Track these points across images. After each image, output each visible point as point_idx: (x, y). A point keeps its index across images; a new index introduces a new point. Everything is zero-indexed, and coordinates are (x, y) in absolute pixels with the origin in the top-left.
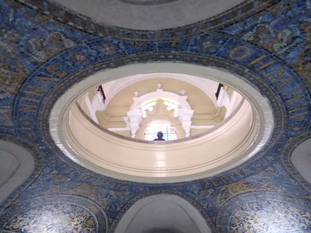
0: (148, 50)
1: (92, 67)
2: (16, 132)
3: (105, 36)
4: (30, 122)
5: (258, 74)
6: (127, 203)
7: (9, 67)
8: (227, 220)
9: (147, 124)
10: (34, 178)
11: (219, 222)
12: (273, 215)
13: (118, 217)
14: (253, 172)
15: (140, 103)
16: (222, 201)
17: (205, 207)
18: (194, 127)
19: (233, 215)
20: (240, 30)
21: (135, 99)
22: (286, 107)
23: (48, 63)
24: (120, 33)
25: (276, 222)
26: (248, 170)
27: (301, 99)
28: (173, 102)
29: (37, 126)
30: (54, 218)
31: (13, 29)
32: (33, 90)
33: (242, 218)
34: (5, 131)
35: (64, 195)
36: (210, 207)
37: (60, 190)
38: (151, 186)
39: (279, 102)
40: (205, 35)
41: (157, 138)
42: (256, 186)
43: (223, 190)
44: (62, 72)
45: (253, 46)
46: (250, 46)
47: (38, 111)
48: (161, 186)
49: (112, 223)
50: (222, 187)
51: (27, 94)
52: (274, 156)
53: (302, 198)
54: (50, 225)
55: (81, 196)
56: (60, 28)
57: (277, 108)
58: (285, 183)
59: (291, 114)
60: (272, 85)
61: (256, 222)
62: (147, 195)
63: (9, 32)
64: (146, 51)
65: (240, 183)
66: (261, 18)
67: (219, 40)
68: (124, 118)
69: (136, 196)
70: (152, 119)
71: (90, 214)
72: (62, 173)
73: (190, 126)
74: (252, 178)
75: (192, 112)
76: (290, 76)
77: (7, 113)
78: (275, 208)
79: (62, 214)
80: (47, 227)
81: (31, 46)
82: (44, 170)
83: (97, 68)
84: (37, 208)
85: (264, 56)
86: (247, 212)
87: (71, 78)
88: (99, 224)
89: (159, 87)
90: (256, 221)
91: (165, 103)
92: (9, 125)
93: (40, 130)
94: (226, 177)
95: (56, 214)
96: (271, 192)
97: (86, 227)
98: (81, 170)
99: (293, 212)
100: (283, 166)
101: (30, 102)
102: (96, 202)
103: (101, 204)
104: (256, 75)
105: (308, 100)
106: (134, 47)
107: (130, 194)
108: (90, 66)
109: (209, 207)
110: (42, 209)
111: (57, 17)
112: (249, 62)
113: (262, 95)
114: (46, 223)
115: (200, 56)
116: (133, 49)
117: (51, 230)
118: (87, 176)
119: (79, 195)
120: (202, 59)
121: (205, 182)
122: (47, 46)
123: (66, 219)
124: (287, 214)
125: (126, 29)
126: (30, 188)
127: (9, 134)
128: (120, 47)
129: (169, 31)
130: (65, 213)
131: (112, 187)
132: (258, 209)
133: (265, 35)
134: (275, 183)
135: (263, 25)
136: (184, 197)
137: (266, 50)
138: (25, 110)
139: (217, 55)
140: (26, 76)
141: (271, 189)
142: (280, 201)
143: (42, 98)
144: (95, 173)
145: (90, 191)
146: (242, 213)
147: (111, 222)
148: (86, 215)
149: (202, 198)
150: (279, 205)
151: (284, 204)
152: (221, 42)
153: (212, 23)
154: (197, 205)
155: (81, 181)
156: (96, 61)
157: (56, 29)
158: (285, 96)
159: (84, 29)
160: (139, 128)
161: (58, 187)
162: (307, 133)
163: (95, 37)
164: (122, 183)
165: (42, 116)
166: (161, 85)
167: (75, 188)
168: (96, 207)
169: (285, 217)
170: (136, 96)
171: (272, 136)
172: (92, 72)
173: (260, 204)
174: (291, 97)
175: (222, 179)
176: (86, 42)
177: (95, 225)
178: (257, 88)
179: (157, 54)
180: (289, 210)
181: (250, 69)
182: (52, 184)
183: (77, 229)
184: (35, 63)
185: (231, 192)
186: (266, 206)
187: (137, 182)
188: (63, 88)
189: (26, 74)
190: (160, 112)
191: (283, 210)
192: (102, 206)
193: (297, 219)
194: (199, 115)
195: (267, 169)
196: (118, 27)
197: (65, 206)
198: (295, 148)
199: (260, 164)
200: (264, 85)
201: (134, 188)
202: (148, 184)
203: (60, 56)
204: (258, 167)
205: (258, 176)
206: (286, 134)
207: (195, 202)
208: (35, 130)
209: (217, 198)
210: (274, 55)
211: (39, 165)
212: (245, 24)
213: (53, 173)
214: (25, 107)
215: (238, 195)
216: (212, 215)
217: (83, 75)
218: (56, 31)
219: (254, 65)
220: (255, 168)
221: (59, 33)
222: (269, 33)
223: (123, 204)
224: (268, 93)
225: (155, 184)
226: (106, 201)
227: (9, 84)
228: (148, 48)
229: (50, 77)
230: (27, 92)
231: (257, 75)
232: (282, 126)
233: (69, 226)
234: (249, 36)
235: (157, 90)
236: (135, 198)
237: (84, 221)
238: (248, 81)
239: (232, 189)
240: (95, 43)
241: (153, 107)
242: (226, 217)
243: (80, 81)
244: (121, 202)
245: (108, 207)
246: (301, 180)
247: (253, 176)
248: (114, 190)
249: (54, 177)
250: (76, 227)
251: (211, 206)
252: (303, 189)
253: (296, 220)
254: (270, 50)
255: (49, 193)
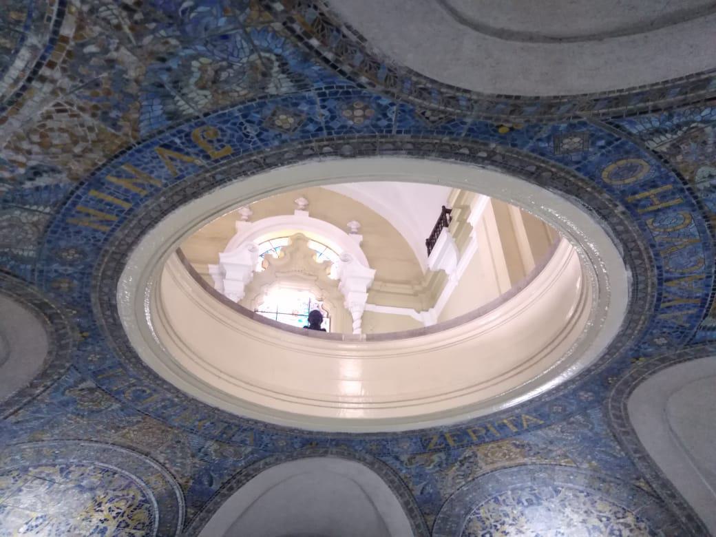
0: (443, 130)
1: (300, 146)
2: (33, 275)
3: (370, 84)
4: (82, 253)
5: (637, 220)
6: (240, 473)
7: (105, 113)
8: (458, 524)
9: (264, 289)
10: (30, 395)
11: (440, 529)
12: (559, 517)
13: (210, 506)
14: (541, 422)
15: (253, 236)
16: (458, 481)
17: (417, 493)
18: (371, 308)
19: (475, 513)
20: (653, 127)
21: (240, 225)
22: (660, 294)
23: (205, 119)
24: (408, 85)
25: (562, 531)
26: (531, 418)
27: (695, 282)
28: (330, 245)
29: (91, 266)
30: (52, 500)
31: (175, 27)
32: (129, 177)
33: (492, 521)
34: (7, 268)
35: (93, 444)
36: (429, 493)
37: (86, 432)
38: (308, 436)
39: (650, 284)
40: (579, 123)
41: (307, 324)
42: (538, 453)
43: (465, 458)
44: (223, 146)
45: (658, 164)
46: (654, 161)
47: (113, 230)
48: (329, 437)
49: (192, 520)
50: (464, 451)
51: (111, 183)
52: (594, 392)
53: (626, 484)
54: (37, 518)
55: (134, 450)
56: (282, 47)
57: (640, 295)
58: (599, 451)
59: (662, 309)
60: (653, 246)
61: (521, 532)
62: (291, 457)
63: (163, 33)
64: (438, 133)
65: (506, 446)
66: (706, 112)
67: (600, 138)
68: (210, 266)
69: (264, 458)
71: (144, 496)
72: (104, 387)
73: (364, 304)
74: (535, 436)
75: (371, 273)
76: (697, 233)
77: (35, 224)
78: (567, 503)
79: (76, 491)
80: (27, 523)
81: (191, 73)
82: (63, 378)
83: (309, 152)
84: (15, 474)
85: (669, 187)
86: (505, 508)
87: (236, 163)
88: (159, 521)
89: (301, 207)
90: (521, 529)
91: (312, 245)
92: (26, 254)
93: (95, 278)
94: (480, 429)
95: (58, 492)
96: (566, 469)
97: (128, 526)
98: (153, 386)
99: (600, 512)
100: (606, 415)
101: (108, 204)
102: (167, 466)
103: (177, 471)
104: (632, 222)
105: (708, 286)
106: (417, 118)
107: (252, 453)
108: (295, 143)
109: (425, 492)
110: (25, 476)
111: (292, 20)
112: (634, 193)
113: (625, 263)
114: (28, 512)
115: (542, 165)
116: (413, 123)
117: (37, 533)
118: (163, 400)
119: (129, 448)
120: (546, 170)
121: (431, 437)
122: (227, 81)
123: (83, 504)
124: (588, 516)
125: (426, 78)
126: (13, 419)
127: (15, 276)
128: (389, 115)
129: (511, 102)
130: (82, 489)
131: (216, 432)
132: (530, 503)
133: (693, 145)
134: (580, 449)
135: (701, 125)
136: (376, 466)
137: (679, 175)
138: (84, 223)
139: (578, 169)
140: (132, 141)
141: (568, 462)
142: (581, 488)
143: (141, 200)
144: (185, 396)
145: (158, 439)
146: (494, 509)
147: (191, 516)
148: (133, 498)
149: (414, 472)
150: (577, 497)
151: (588, 495)
152: (602, 143)
153: (610, 102)
154: (400, 486)
155: (145, 413)
156: (313, 136)
157: (273, 47)
158: (667, 272)
159: (337, 61)
160: (244, 294)
161: (84, 422)
162: (678, 352)
163: (348, 81)
164: (242, 424)
165: (117, 243)
166: (306, 202)
167: (124, 428)
168: (163, 477)
169: (584, 521)
170: (244, 217)
171: (607, 351)
172: (292, 159)
173: (536, 492)
174: (679, 276)
175: (471, 434)
176: (321, 89)
177: (151, 523)
178: (622, 250)
179: (457, 143)
180: (594, 507)
181: (627, 208)
182: (73, 413)
183: (103, 531)
184: (173, 115)
185: (481, 463)
186: (549, 496)
187: (277, 426)
188: (204, 183)
189: (135, 138)
190: (296, 263)
191: (582, 506)
192: (178, 477)
193: (606, 526)
194: (385, 281)
195: (572, 419)
196: (410, 71)
197: (88, 471)
198: (644, 379)
199: (560, 406)
200: (637, 245)
201: (266, 439)
202: (302, 432)
203: (240, 110)
204: (554, 413)
205: (550, 432)
206: (636, 351)
207: (396, 479)
208: (83, 274)
209: (447, 475)
210: (689, 189)
211: (57, 363)
212: (670, 117)
213: (83, 385)
214: (88, 215)
215: (496, 470)
216: (427, 511)
217: (268, 161)
218: (269, 51)
219: (639, 201)
220: (549, 415)
221: (273, 58)
222: (705, 143)
223: (229, 475)
224: (638, 262)
225: (318, 433)
226: (191, 465)
227: (81, 154)
228: (446, 128)
229: (188, 154)
230: (114, 180)
231: (635, 224)
232: (636, 332)
233: (84, 523)
234: (661, 143)
235: (296, 212)
236: (262, 462)
237: (124, 512)
238: (611, 232)
239: (486, 455)
240: (338, 96)
241: (282, 250)
242: (458, 516)
243: (253, 173)
244: (226, 469)
245: (192, 481)
246: (634, 447)
247: (539, 432)
248: (217, 440)
249: (83, 396)
250: (102, 526)
251: (431, 491)
252: (633, 464)
253: (603, 529)
254: (687, 178)
255: (56, 437)
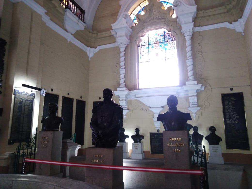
18: (197, 29)
70: (144, 26)
